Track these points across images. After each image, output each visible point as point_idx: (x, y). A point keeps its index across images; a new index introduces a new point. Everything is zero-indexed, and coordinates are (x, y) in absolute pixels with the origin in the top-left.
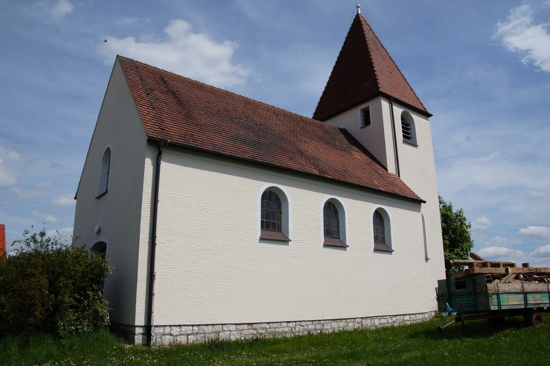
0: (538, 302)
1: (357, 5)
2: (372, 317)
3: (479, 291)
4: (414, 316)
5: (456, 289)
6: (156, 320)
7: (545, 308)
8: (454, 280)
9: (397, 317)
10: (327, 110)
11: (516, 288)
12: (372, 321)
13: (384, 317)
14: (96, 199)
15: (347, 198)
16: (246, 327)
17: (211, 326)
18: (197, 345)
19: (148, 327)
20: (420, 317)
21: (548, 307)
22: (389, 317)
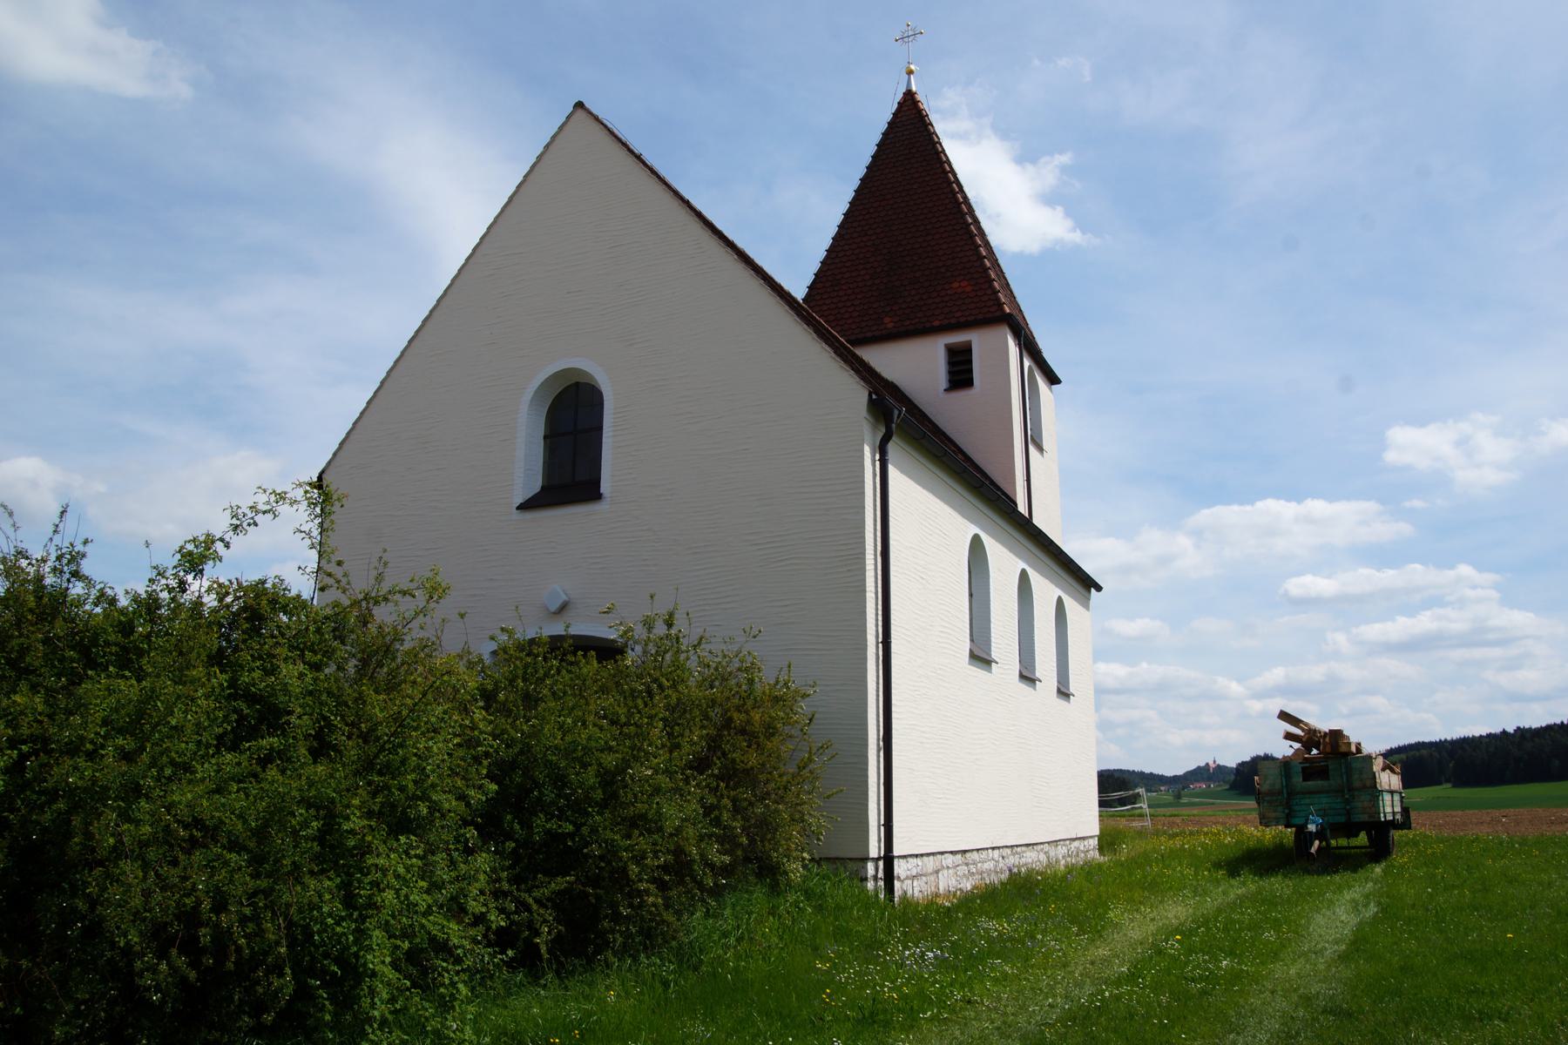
1: (909, 67)
3: (1357, 784)
5: (1304, 780)
6: (897, 850)
8: (1300, 763)
14: (1284, 716)
15: (1076, 600)
18: (1345, 869)
19: (889, 859)
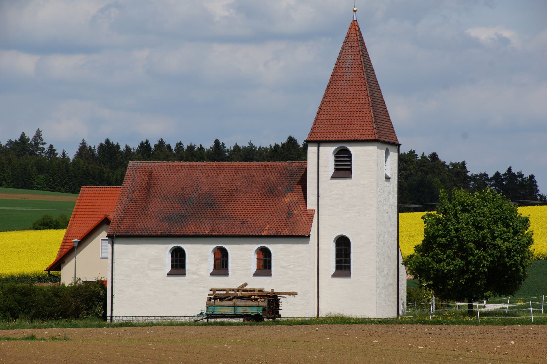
16: (159, 318)
17: (142, 317)
19: (111, 317)
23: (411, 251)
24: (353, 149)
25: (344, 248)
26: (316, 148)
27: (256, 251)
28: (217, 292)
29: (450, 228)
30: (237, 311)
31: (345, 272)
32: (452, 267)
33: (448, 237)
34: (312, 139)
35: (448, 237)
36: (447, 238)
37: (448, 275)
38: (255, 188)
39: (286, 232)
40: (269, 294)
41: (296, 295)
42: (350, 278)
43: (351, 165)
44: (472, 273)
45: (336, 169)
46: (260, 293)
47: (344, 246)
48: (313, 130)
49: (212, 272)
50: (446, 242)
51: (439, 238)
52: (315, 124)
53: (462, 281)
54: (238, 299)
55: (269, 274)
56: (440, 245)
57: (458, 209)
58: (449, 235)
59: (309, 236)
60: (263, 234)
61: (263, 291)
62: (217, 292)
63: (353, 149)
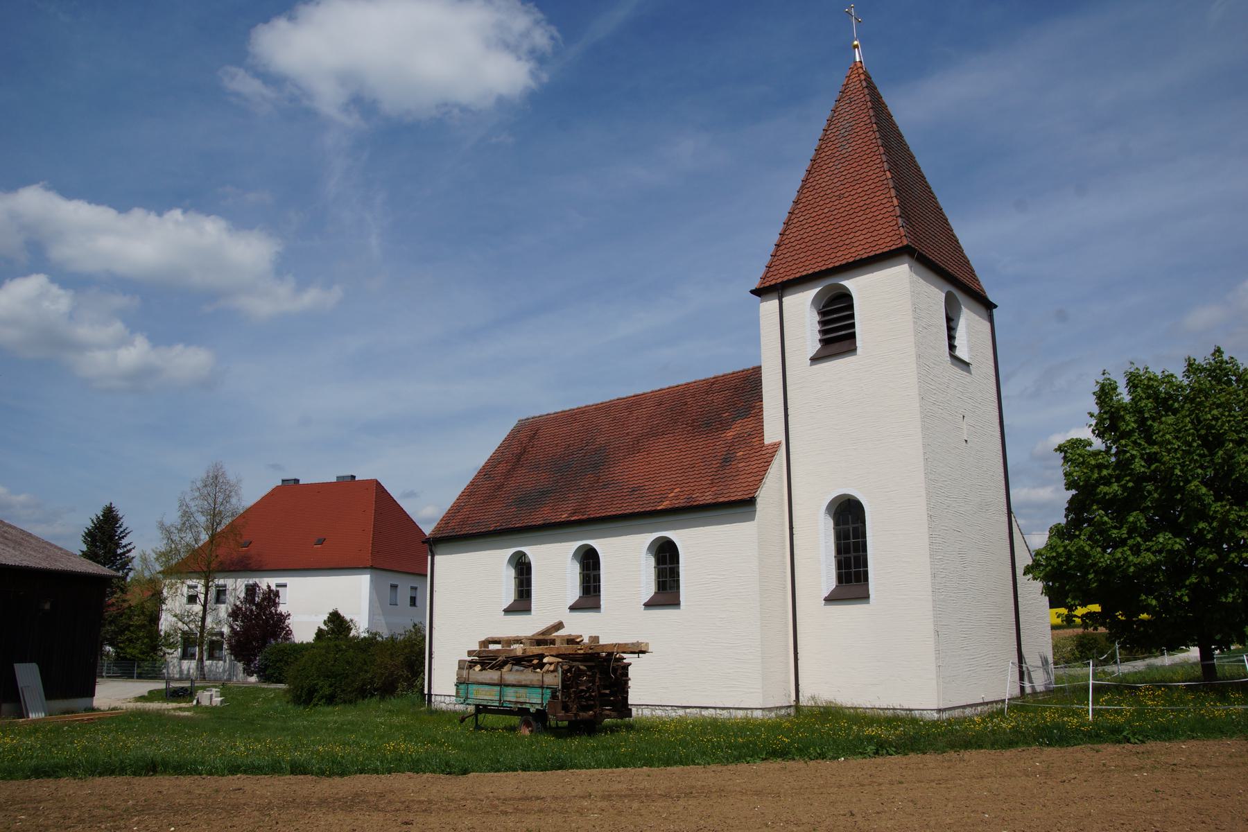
0: (521, 700)
2: (640, 705)
4: (725, 711)
7: (532, 710)
9: (688, 710)
10: (877, 177)
11: (491, 679)
12: (640, 710)
13: (660, 708)
19: (430, 695)
20: (740, 714)
21: (537, 709)
22: (670, 708)
23: (1039, 540)
24: (853, 284)
25: (854, 529)
26: (777, 301)
27: (650, 549)
28: (492, 647)
29: (1128, 454)
30: (506, 699)
31: (854, 588)
32: (1148, 558)
33: (1128, 478)
34: (767, 284)
35: (1128, 478)
36: (1123, 482)
37: (1143, 580)
38: (680, 424)
39: (708, 498)
40: (580, 652)
41: (644, 652)
42: (869, 603)
43: (853, 325)
44: (1210, 569)
45: (825, 342)
46: (570, 649)
47: (853, 523)
48: (769, 267)
49: (507, 608)
50: (1124, 491)
51: (1102, 487)
52: (775, 256)
53: (1184, 595)
54: (513, 664)
55: (864, 597)
56: (1107, 504)
57: (1146, 406)
58: (1129, 475)
59: (750, 502)
60: (659, 508)
61: (578, 643)
62: (492, 647)
63: (853, 284)
